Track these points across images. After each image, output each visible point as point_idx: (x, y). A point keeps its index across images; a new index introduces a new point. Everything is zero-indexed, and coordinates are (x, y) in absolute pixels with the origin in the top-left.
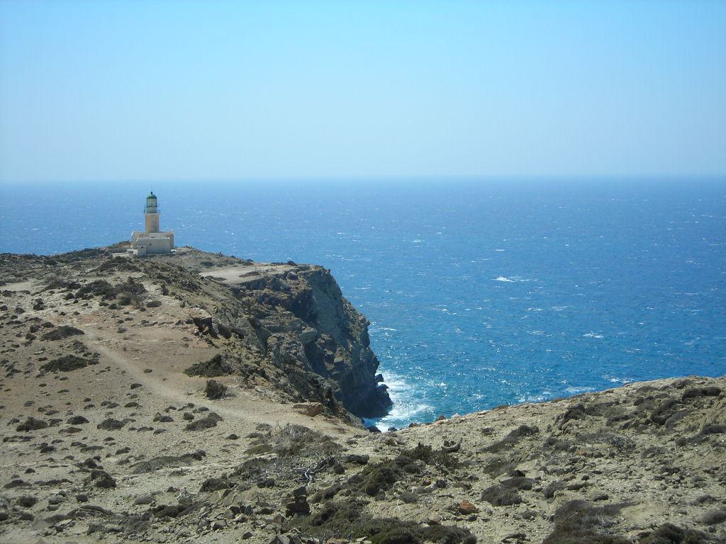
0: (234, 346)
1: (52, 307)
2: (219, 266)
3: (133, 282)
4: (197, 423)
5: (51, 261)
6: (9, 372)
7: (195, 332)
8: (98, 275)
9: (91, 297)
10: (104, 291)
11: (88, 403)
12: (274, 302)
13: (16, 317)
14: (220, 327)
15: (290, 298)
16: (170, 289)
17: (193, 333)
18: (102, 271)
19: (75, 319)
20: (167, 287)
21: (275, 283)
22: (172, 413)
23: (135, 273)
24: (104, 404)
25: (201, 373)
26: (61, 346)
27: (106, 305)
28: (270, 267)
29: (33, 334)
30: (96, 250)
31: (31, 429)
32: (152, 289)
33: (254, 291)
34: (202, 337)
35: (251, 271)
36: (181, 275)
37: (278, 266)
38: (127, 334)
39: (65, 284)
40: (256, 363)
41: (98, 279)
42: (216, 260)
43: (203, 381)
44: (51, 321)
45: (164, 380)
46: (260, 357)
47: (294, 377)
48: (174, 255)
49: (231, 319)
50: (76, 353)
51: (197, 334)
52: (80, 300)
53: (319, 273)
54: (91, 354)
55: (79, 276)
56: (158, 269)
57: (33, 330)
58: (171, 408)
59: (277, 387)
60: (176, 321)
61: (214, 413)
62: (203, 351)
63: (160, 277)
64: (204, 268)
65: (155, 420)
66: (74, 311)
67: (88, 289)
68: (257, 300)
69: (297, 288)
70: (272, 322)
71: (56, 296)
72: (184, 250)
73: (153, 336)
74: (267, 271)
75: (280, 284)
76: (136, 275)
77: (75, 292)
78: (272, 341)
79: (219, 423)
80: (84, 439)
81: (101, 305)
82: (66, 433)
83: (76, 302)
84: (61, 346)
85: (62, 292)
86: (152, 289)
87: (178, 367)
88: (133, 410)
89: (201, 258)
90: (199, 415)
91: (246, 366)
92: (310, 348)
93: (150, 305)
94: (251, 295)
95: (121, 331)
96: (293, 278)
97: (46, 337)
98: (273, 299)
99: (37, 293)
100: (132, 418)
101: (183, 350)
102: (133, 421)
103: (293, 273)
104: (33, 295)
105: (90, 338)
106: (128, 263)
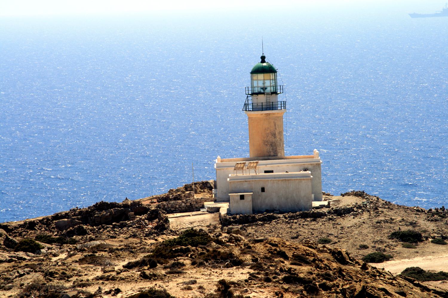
8: (144, 277)
18: (153, 266)
23: (233, 270)
30: (126, 206)
36: (340, 271)
41: (147, 285)
48: (321, 215)
55: (101, 278)
56: (286, 258)
64: (399, 248)
72: (350, 201)
106: (214, 244)
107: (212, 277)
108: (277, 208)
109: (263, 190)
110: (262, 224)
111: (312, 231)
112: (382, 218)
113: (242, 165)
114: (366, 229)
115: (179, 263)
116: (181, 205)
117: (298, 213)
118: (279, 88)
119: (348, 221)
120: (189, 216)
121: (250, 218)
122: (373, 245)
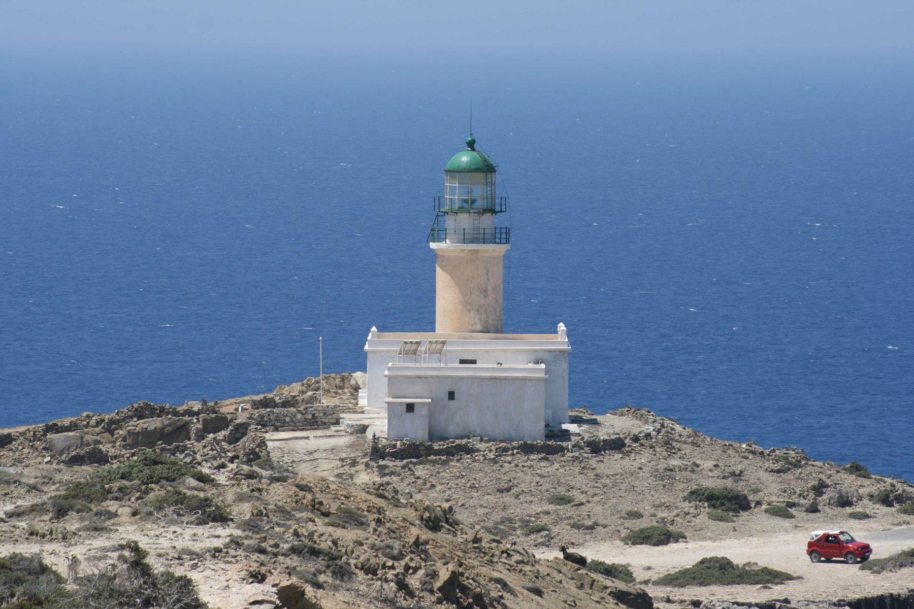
18: (61, 513)
64: (703, 519)
107: (161, 540)
108: (479, 431)
109: (451, 396)
110: (444, 461)
111: (538, 479)
112: (674, 462)
113: (414, 347)
114: (644, 481)
115: (108, 512)
116: (295, 416)
117: (515, 444)
118: (498, 201)
119: (613, 463)
120: (307, 438)
121: (423, 448)
122: (652, 511)
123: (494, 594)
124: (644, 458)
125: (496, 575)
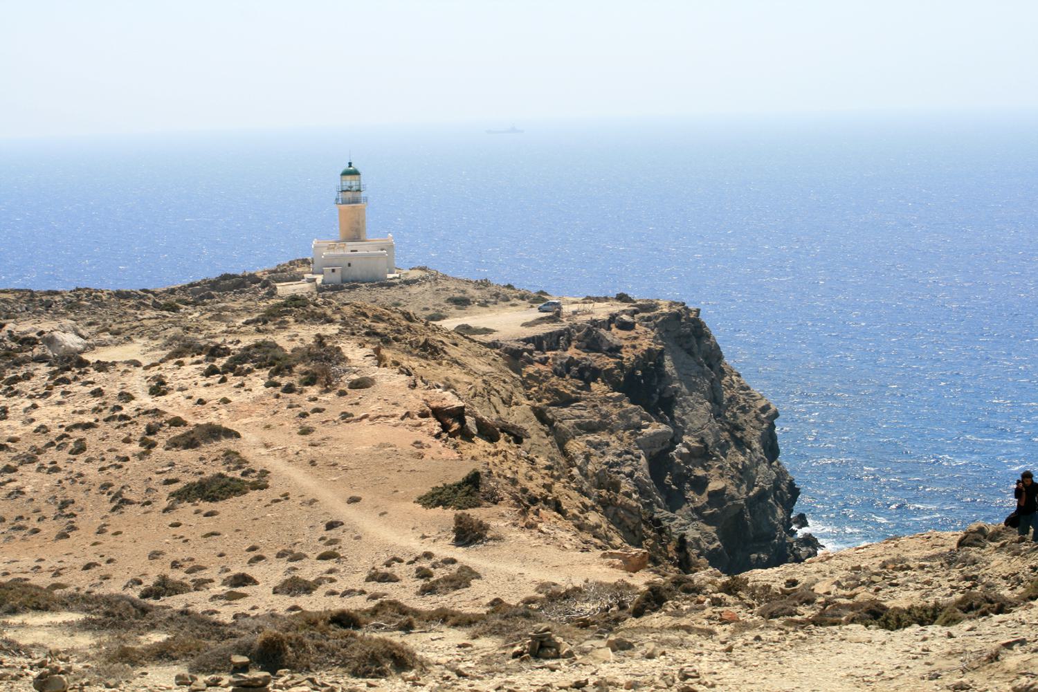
0: (505, 457)
1: (181, 389)
2: (481, 305)
3: (324, 345)
4: (438, 581)
5: (168, 302)
6: (114, 504)
7: (436, 432)
8: (259, 331)
9: (249, 371)
10: (271, 360)
11: (252, 554)
12: (588, 375)
13: (120, 408)
14: (480, 422)
15: (620, 366)
16: (387, 353)
17: (431, 434)
18: (265, 322)
19: (223, 411)
20: (384, 352)
21: (591, 338)
22: (397, 569)
24: (280, 555)
25: (444, 504)
26: (201, 459)
27: (276, 385)
28: (581, 307)
29: (151, 438)
31: (163, 595)
32: (356, 354)
33: (549, 354)
34: (446, 441)
35: (173, 485)
37: (597, 305)
38: (316, 437)
39: (201, 348)
40: (544, 486)
41: (260, 338)
42: (477, 293)
43: (448, 515)
44: (181, 415)
45: (382, 514)
46: (552, 476)
47: (616, 514)
48: (394, 285)
49: (501, 408)
50: (229, 469)
51: (438, 436)
52: (230, 376)
53: (677, 316)
54: (254, 471)
56: (367, 317)
57: (151, 430)
58: (395, 559)
59: (580, 528)
60: (401, 411)
61: (467, 567)
62: (450, 461)
63: (372, 333)
65: (368, 580)
66: (221, 396)
67: (245, 355)
68: (555, 372)
69: (634, 347)
70: (585, 413)
71: (189, 369)
72: (416, 274)
73: (364, 437)
74: (575, 313)
75: (600, 337)
76: (331, 330)
77: (220, 362)
78: (576, 446)
79: (474, 583)
80: (254, 608)
81: (267, 386)
82: (223, 601)
83: (223, 380)
84: (201, 459)
85: (198, 362)
86: (356, 354)
87: (406, 493)
88: (330, 564)
89: (447, 289)
90: (443, 571)
91: (525, 490)
92: (659, 461)
93: (357, 385)
94: (544, 362)
95: (305, 431)
96: (626, 326)
97: (174, 444)
98: (587, 368)
99: (154, 365)
100: (330, 576)
101: (413, 464)
102: (332, 581)
103: (625, 317)
104: (146, 368)
105: (250, 445)
106: (312, 306)
109: (349, 265)
123: (440, 347)
124: (428, 285)
125: (439, 339)
